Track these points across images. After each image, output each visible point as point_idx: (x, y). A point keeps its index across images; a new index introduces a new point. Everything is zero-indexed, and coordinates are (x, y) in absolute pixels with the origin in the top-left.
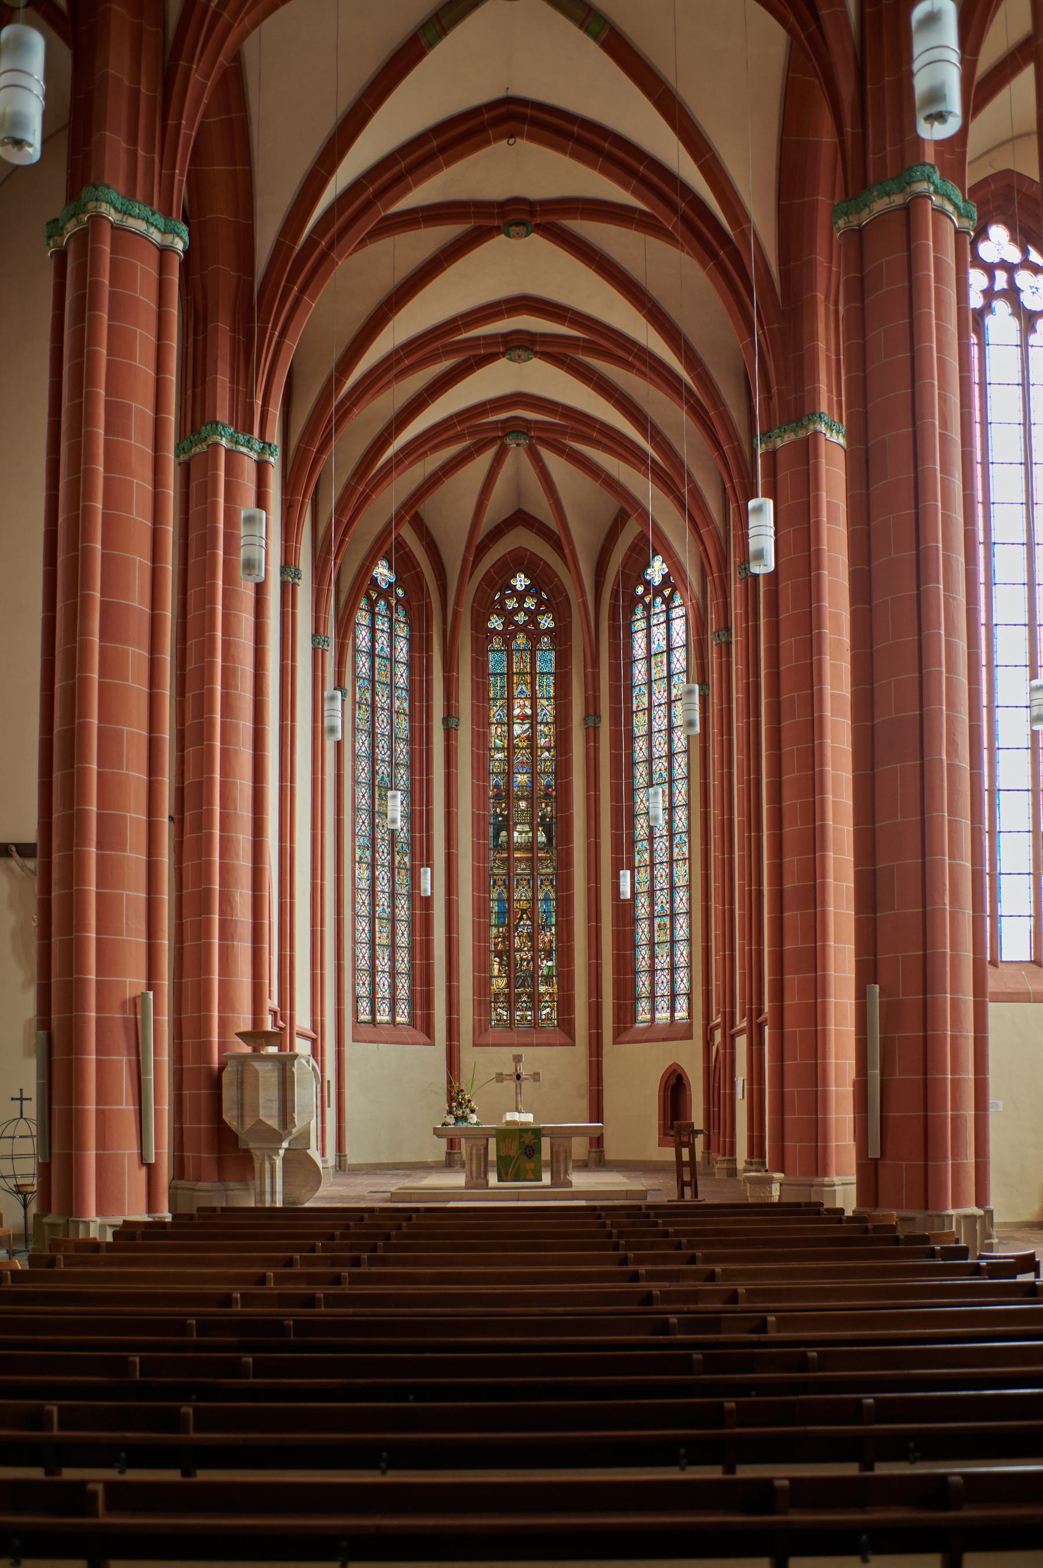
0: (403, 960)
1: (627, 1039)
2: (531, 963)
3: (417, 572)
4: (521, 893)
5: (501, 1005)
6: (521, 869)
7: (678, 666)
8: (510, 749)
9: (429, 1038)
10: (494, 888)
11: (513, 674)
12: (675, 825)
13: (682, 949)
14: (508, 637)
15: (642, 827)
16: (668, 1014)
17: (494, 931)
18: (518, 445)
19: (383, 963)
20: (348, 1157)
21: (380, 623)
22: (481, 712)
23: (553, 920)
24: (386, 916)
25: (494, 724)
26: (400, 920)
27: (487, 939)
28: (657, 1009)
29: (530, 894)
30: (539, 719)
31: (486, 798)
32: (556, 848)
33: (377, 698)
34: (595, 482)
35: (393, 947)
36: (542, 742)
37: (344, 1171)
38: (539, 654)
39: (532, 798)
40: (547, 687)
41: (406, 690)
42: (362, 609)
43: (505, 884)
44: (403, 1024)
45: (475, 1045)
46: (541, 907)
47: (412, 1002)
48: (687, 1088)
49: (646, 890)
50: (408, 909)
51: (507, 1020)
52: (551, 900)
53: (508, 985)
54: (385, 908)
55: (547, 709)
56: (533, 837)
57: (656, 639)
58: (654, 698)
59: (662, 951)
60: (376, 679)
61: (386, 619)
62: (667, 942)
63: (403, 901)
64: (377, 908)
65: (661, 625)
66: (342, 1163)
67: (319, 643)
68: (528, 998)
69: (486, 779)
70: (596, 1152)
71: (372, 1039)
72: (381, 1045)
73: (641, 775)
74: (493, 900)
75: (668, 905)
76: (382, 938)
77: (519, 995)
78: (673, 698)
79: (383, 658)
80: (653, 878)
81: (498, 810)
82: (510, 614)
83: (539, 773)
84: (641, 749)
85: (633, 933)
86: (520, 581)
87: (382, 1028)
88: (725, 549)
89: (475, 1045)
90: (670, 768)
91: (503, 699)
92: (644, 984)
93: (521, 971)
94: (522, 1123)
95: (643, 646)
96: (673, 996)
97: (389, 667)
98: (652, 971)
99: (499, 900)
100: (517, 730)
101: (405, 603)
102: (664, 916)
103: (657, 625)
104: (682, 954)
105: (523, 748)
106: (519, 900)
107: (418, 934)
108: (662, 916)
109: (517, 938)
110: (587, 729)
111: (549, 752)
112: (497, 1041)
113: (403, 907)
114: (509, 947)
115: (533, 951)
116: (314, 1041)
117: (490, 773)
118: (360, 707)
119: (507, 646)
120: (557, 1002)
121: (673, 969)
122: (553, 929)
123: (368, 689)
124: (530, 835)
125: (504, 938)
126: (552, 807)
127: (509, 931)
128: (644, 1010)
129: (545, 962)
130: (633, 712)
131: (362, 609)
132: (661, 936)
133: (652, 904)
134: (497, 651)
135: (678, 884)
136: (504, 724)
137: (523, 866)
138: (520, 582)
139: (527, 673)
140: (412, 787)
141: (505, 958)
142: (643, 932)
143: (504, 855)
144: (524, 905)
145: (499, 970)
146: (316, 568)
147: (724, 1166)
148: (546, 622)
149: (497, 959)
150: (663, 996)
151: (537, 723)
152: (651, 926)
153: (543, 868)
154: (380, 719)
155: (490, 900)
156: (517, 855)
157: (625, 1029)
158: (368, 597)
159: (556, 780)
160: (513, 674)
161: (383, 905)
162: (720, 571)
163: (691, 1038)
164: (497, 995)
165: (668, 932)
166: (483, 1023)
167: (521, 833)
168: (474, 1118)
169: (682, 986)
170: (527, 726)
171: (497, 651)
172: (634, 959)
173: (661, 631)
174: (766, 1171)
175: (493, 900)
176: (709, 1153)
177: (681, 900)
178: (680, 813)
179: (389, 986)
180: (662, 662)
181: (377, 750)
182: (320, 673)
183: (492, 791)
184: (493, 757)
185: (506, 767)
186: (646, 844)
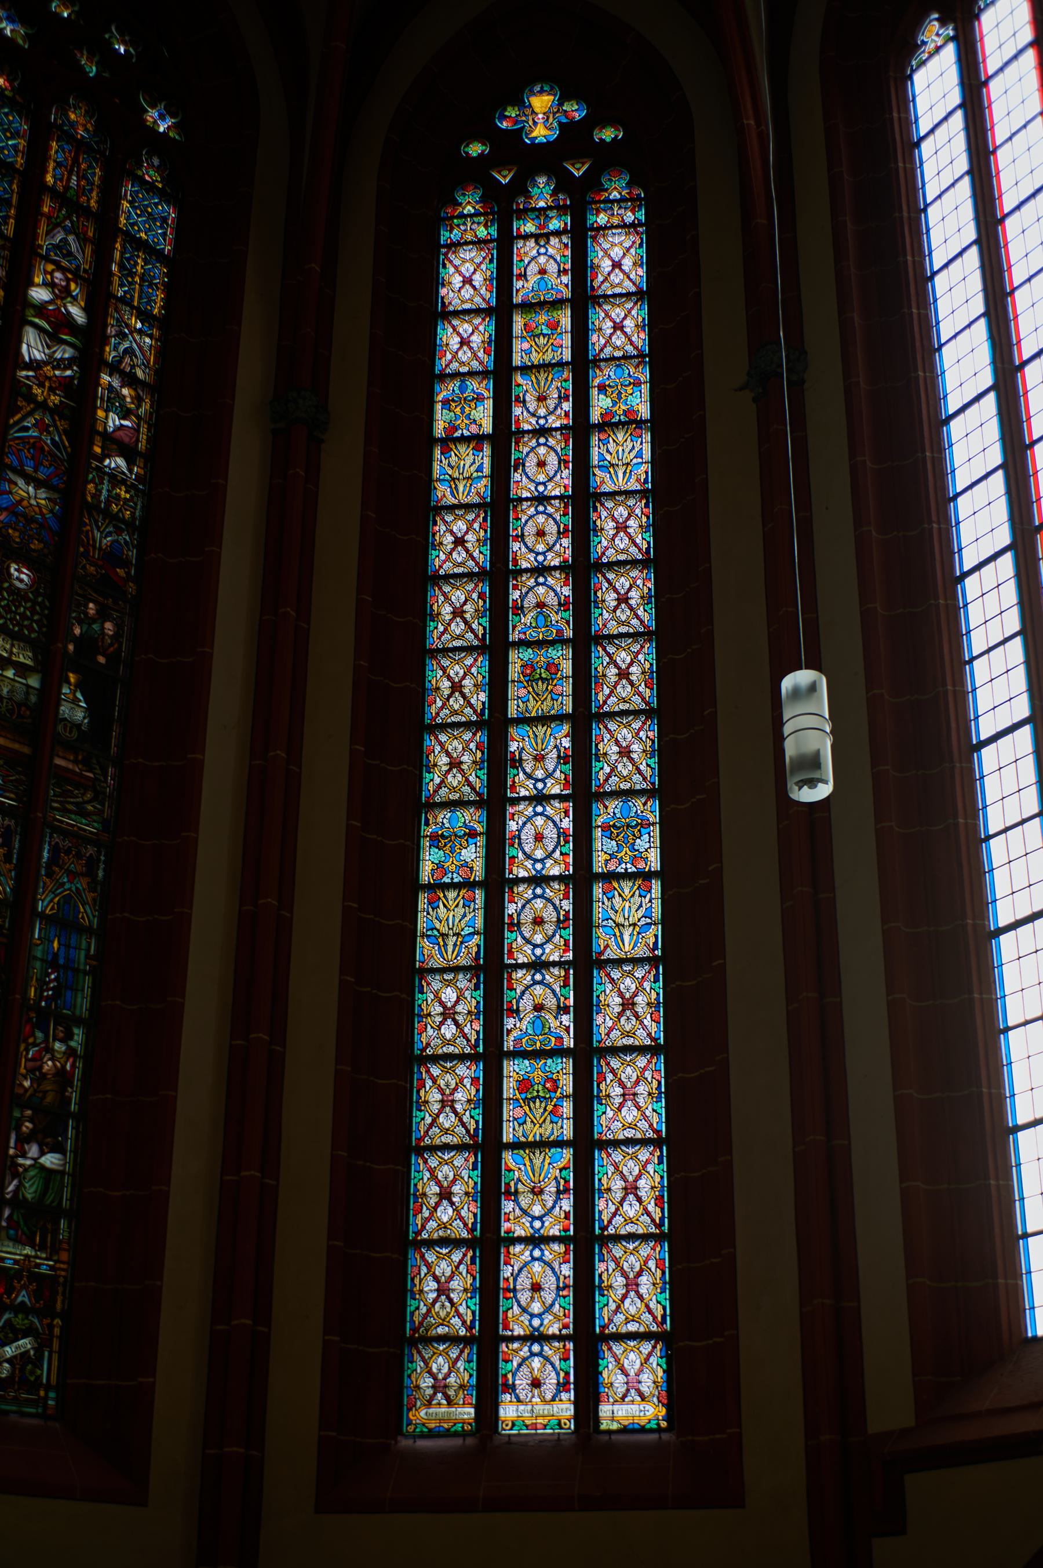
23: (83, 1004)
52: (81, 930)
56: (42, 691)
111: (130, 463)
122: (79, 1034)
126: (119, 626)
129: (33, 1150)
130: (433, 441)
153: (65, 812)
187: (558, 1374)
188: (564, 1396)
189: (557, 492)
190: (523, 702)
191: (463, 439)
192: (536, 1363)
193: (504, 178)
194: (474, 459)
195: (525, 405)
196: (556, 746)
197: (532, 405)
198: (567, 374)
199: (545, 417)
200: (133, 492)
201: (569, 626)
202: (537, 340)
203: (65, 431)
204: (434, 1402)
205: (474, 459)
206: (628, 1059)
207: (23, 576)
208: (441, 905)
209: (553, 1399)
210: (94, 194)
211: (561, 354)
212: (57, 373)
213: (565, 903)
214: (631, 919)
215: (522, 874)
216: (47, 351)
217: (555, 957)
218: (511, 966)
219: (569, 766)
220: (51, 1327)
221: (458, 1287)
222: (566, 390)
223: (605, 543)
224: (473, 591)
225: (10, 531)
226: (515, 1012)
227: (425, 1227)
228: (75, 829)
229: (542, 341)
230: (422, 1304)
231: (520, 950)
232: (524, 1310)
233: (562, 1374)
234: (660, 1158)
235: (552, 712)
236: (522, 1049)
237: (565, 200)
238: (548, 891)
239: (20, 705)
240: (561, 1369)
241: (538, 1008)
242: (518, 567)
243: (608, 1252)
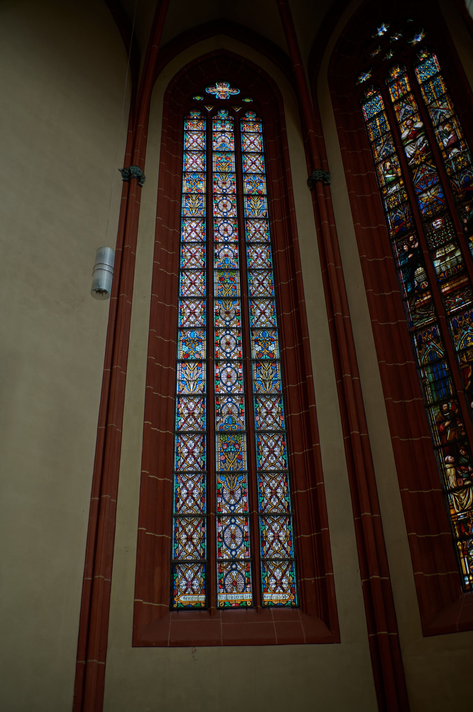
17: (435, 412)
45: (427, 632)
72: (201, 650)
81: (405, 248)
89: (427, 632)
145: (457, 476)
149: (449, 458)
155: (419, 368)
167: (442, 259)
174: (194, 593)
183: (393, 230)
187: (245, 579)
189: (231, 216)
190: (220, 291)
191: (192, 361)
192: (234, 573)
193: (209, 109)
194: (198, 372)
195: (217, 185)
196: (240, 487)
197: (220, 185)
198: (234, 176)
199: (227, 237)
200: (464, 155)
201: (244, 424)
202: (225, 285)
203: (431, 164)
204: (187, 593)
205: (198, 372)
206: (275, 519)
207: (438, 223)
208: (191, 199)
209: (243, 591)
210: (408, 86)
211: (236, 292)
212: (420, 150)
213: (235, 226)
214: (269, 378)
215: (222, 392)
216: (414, 147)
217: (237, 392)
218: (218, 395)
219: (249, 542)
221: (196, 537)
222: (245, 489)
223: (248, 167)
224: (199, 304)
225: (428, 213)
226: (220, 414)
227: (180, 555)
228: (425, 324)
229: (227, 286)
230: (180, 545)
231: (224, 506)
233: (246, 579)
234: (289, 522)
235: (233, 296)
236: (223, 430)
237: (232, 118)
238: (234, 400)
239: (456, 266)
240: (246, 576)
242: (221, 512)
243: (267, 567)
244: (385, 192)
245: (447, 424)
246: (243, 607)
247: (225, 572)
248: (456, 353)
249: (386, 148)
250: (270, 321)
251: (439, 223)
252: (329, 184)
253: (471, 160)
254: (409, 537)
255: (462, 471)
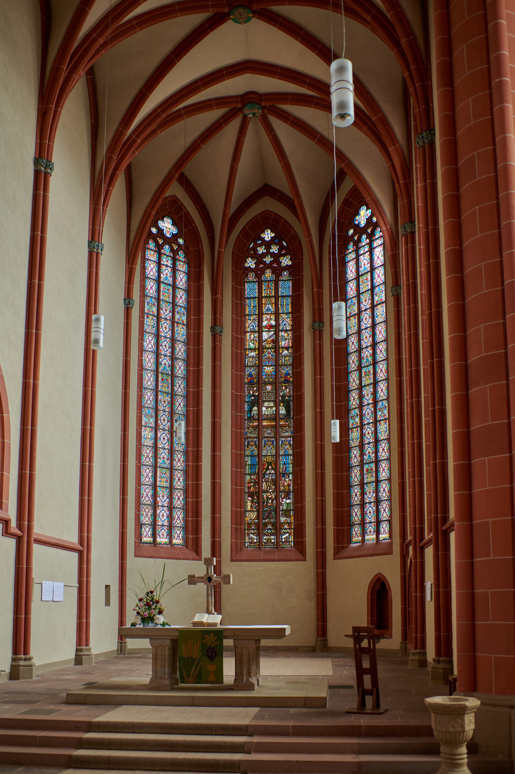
0: (179, 499)
1: (344, 555)
2: (275, 501)
3: (179, 205)
4: (268, 451)
5: (252, 532)
6: (268, 433)
7: (379, 280)
8: (260, 349)
9: (198, 555)
10: (248, 447)
11: (262, 297)
12: (378, 395)
13: (384, 486)
14: (259, 272)
15: (354, 399)
16: (374, 536)
17: (248, 478)
18: (254, 114)
19: (163, 500)
20: (128, 644)
21: (165, 260)
22: (239, 324)
23: (291, 470)
24: (165, 466)
25: (249, 332)
26: (177, 470)
27: (242, 484)
28: (366, 533)
29: (274, 451)
30: (281, 328)
31: (242, 384)
32: (293, 418)
33: (161, 311)
34: (312, 142)
35: (171, 488)
36: (283, 344)
37: (125, 654)
38: (280, 283)
39: (276, 383)
40: (286, 305)
41: (185, 308)
42: (151, 250)
43: (256, 444)
44: (178, 545)
45: (232, 560)
46: (282, 460)
47: (185, 529)
48: (389, 593)
49: (358, 444)
50: (183, 461)
51: (256, 543)
52: (289, 455)
53: (258, 517)
54: (165, 460)
55: (286, 322)
56: (276, 410)
57: (363, 264)
58: (361, 305)
59: (370, 489)
60: (161, 298)
61: (169, 258)
62: (373, 482)
63: (179, 456)
64: (159, 460)
65: (366, 254)
66: (123, 648)
67: (94, 248)
68: (273, 526)
69: (243, 370)
70: (321, 640)
71: (151, 555)
73: (353, 362)
74: (247, 456)
75: (374, 455)
76: (163, 482)
77: (266, 525)
78: (375, 304)
79: (167, 284)
80: (362, 435)
81: (251, 392)
82: (260, 257)
83: (281, 366)
84: (353, 343)
85: (349, 477)
86: (268, 234)
87: (160, 546)
88: (408, 162)
89: (232, 560)
90: (374, 354)
91: (255, 315)
92: (356, 515)
93: (267, 507)
94: (209, 624)
95: (353, 270)
96: (378, 522)
97: (171, 291)
98: (363, 505)
99: (252, 456)
100: (265, 335)
101: (186, 249)
102: (371, 463)
103: (363, 254)
104: (384, 490)
105: (269, 348)
106: (266, 456)
107: (190, 479)
108: (369, 463)
109: (264, 483)
110: (314, 332)
111: (288, 350)
112: (248, 558)
113: (179, 460)
114: (259, 490)
115: (276, 492)
116: (81, 553)
117: (245, 366)
118: (147, 317)
119: (258, 278)
120: (293, 529)
121: (378, 502)
122: (291, 476)
123: (154, 305)
124: (274, 409)
125: (255, 483)
126: (290, 389)
127: (258, 478)
128: (356, 534)
129: (284, 500)
131: (151, 250)
132: (369, 478)
133: (362, 455)
134: (251, 282)
135: (381, 438)
136: (256, 332)
137: (269, 431)
138: (268, 235)
139: (272, 297)
140: (187, 376)
141: (256, 498)
142: (356, 476)
143: (255, 424)
144: (270, 459)
145: (251, 506)
146: (94, 194)
147: (416, 657)
148: (286, 261)
149: (250, 498)
150: (370, 522)
151: (280, 330)
152: (362, 471)
154: (164, 326)
155: (245, 456)
156: (265, 423)
157: (343, 548)
158: (157, 243)
159: (293, 369)
160: (262, 297)
161: (164, 458)
162: (405, 178)
163: (391, 553)
164: (249, 524)
165: (374, 475)
166: (239, 545)
167: (267, 408)
168: (161, 619)
169: (385, 515)
170: (272, 333)
171: (251, 282)
172: (349, 496)
173: (366, 258)
175: (247, 456)
176: (405, 643)
177: (383, 450)
178: (382, 386)
179: (167, 517)
180: (367, 279)
181: (161, 348)
182: (95, 270)
184: (247, 355)
185: (257, 362)
186: (357, 411)
188: (374, 534)
220: (291, 531)
232: (368, 517)
239: (272, 415)
241: (369, 453)
244: (247, 353)
245: (252, 484)
246: (166, 544)
247: (160, 530)
248: (262, 455)
249: (253, 324)
250: (182, 410)
251: (270, 388)
252: (222, 336)
253: (292, 362)
254: (231, 527)
255: (254, 505)
